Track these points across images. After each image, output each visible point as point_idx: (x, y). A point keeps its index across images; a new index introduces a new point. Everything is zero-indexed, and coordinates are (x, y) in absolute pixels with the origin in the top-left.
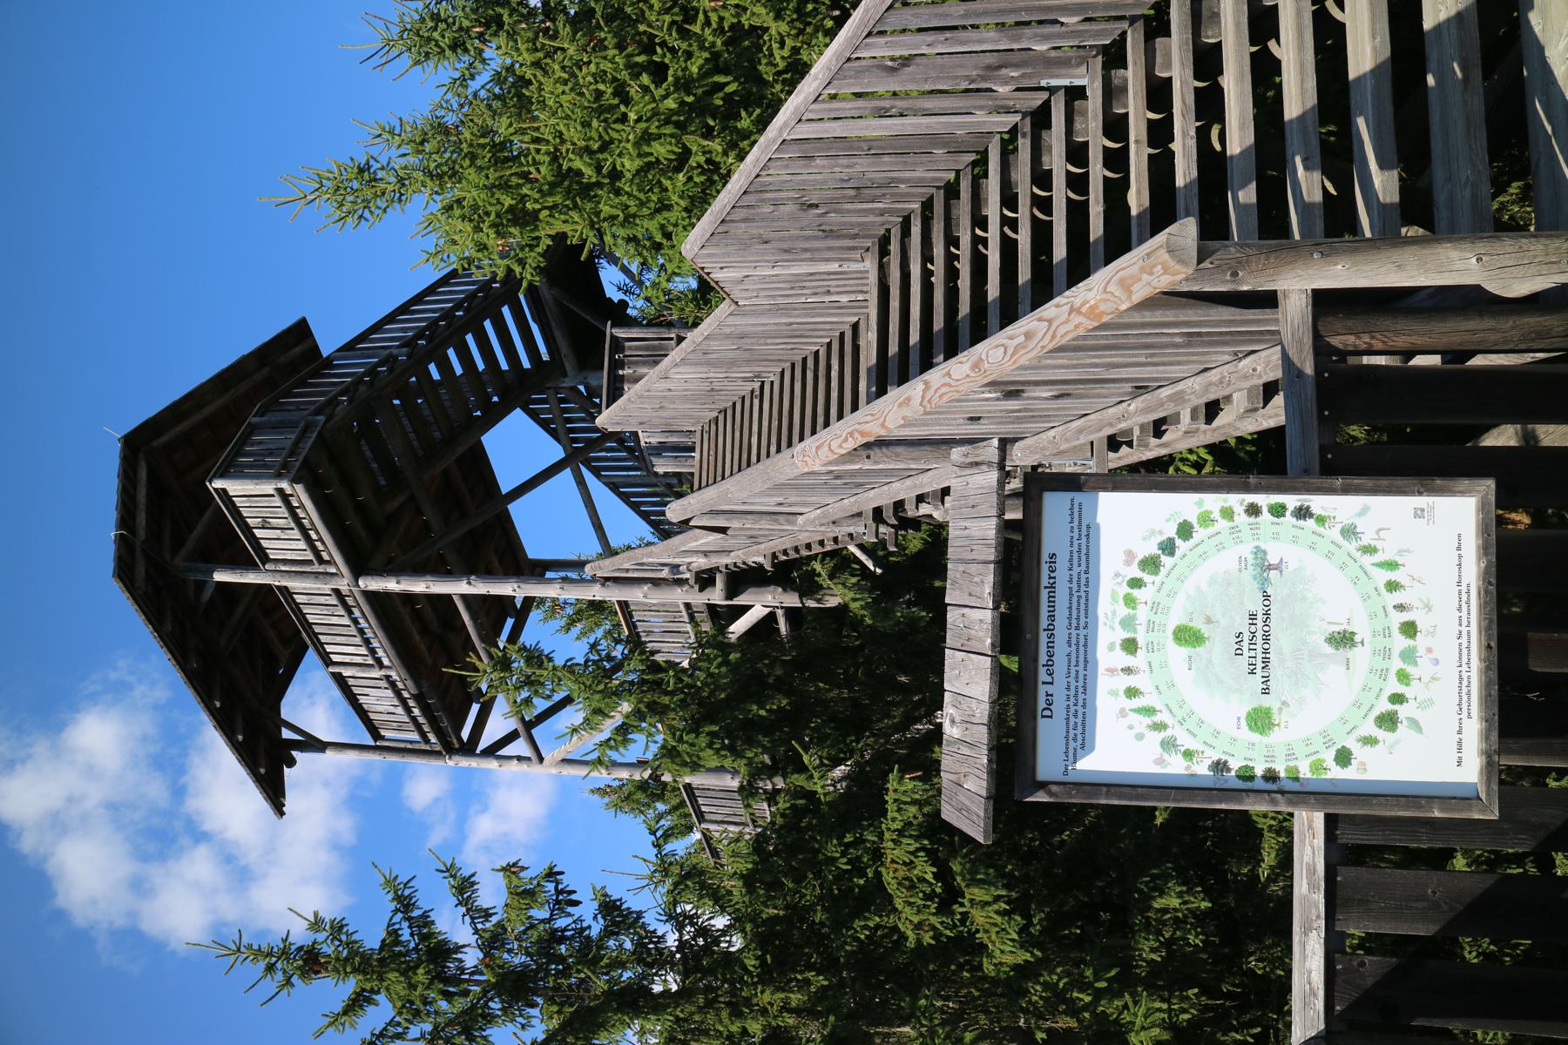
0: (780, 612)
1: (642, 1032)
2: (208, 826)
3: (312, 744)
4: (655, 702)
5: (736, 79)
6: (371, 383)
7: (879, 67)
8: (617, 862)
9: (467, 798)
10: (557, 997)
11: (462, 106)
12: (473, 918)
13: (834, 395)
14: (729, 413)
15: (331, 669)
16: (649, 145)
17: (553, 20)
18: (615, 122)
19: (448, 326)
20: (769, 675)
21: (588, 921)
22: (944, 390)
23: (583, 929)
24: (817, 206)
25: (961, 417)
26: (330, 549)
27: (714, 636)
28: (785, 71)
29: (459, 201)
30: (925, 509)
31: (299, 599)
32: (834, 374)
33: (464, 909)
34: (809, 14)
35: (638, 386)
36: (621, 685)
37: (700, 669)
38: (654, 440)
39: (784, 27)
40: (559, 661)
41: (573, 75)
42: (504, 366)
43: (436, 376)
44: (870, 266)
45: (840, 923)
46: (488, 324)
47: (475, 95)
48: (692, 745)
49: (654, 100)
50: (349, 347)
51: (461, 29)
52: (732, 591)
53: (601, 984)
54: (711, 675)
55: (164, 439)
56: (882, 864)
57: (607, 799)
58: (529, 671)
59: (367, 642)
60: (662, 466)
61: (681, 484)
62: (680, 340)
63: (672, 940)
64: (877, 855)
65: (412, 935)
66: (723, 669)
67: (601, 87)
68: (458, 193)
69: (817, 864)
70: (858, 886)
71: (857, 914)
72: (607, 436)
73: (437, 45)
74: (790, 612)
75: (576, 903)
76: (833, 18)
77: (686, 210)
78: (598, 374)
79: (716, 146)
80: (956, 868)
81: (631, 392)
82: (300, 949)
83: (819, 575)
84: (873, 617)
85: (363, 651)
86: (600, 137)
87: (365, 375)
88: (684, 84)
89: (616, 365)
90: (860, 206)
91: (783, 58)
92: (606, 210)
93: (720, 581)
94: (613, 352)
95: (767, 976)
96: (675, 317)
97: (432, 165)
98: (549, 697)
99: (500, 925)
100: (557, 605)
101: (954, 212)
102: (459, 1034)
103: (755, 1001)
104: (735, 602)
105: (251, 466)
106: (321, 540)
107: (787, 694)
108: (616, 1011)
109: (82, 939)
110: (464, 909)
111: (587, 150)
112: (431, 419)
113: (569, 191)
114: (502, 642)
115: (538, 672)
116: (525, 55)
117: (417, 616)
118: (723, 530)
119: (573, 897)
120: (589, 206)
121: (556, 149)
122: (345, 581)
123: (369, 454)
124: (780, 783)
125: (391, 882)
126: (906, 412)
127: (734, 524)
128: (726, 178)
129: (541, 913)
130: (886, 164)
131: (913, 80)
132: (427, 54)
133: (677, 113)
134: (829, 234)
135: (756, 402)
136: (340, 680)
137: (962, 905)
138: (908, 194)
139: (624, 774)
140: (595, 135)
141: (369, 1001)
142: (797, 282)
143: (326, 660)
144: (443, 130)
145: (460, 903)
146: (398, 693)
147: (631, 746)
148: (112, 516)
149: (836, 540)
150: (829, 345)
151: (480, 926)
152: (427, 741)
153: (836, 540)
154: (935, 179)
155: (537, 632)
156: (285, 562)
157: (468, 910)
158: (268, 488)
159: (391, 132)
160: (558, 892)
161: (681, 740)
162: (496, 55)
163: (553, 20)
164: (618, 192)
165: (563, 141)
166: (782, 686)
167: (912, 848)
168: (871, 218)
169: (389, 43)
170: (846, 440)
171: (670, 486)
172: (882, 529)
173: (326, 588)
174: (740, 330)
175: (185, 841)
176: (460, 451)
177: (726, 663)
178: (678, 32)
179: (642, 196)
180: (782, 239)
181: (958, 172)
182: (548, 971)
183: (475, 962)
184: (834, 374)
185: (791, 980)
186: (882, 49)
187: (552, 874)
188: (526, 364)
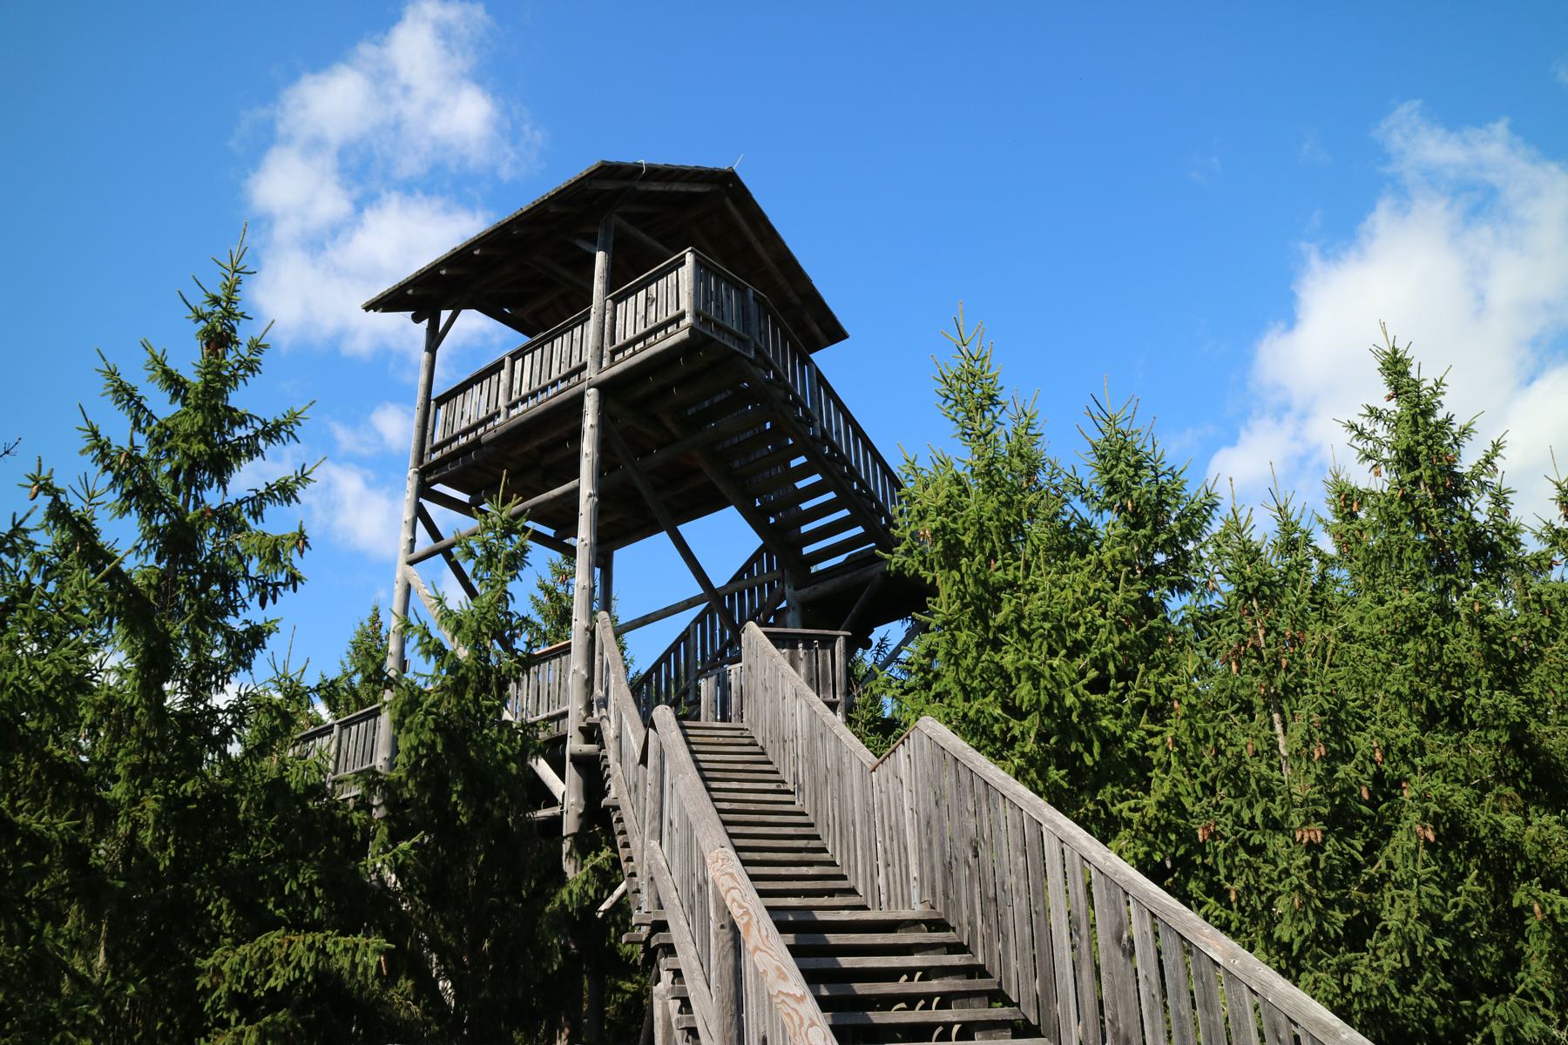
0: (557, 810)
1: (122, 671)
2: (369, 216)
3: (434, 339)
4: (467, 684)
5: (1096, 763)
6: (786, 402)
7: (1121, 924)
8: (305, 641)
9: (377, 468)
10: (167, 581)
11: (1056, 488)
12: (253, 499)
13: (783, 871)
14: (761, 758)
15: (507, 360)
16: (1028, 679)
17: (1143, 578)
18: (1050, 646)
19: (843, 476)
20: (494, 804)
21: (244, 615)
22: (796, 1018)
23: (235, 610)
24: (976, 856)
25: (766, 1028)
26: (625, 362)
27: (534, 746)
28: (1107, 813)
29: (965, 491)
30: (667, 977)
31: (578, 331)
32: (804, 870)
33: (262, 490)
34: (1165, 836)
35: (787, 666)
36: (486, 649)
37: (500, 731)
38: (732, 678)
39: (1151, 812)
40: (511, 587)
41: (1091, 601)
42: (805, 529)
43: (794, 463)
44: (917, 910)
45: (227, 882)
46: (845, 513)
47: (1066, 501)
48: (422, 725)
49: (1073, 682)
50: (821, 380)
51: (1129, 489)
52: (580, 761)
53: (178, 628)
54: (494, 743)
55: (732, 208)
56: (288, 930)
57: (367, 624)
58: (502, 556)
59: (534, 395)
60: (707, 687)
61: (689, 704)
62: (832, 706)
63: (219, 700)
64: (298, 924)
65: (240, 438)
66: (500, 757)
67: (1082, 629)
68: (973, 490)
69: (292, 857)
70: (266, 903)
71: (236, 903)
72: (737, 631)
73: (1113, 467)
74: (557, 821)
75: (263, 604)
76: (1163, 861)
77: (965, 715)
78: (798, 622)
79: (1030, 746)
80: (281, 1016)
81: (780, 657)
82: (233, 329)
83: (597, 855)
84: (553, 913)
85: (525, 391)
86: (1034, 631)
87: (795, 395)
88: (1088, 711)
89: (808, 641)
90: (977, 901)
91: (1121, 811)
92: (963, 636)
93: (591, 748)
94: (821, 638)
95: (174, 806)
96: (857, 700)
97: (999, 466)
98: (475, 576)
99: (245, 527)
100: (566, 576)
101: (975, 1002)
102: (134, 484)
103: (148, 792)
104: (568, 764)
105: (706, 289)
106: (635, 353)
107: (473, 822)
108: (146, 645)
109: (270, 93)
110: (262, 490)
111: (1020, 617)
112: (752, 458)
113: (980, 598)
114: (531, 524)
115: (501, 566)
116: (1109, 554)
117: (559, 443)
118: (644, 760)
119: (269, 601)
120: (966, 618)
121: (1020, 587)
122: (593, 376)
123: (717, 399)
124: (378, 814)
125: (294, 418)
126: (771, 976)
127: (651, 773)
128: (997, 756)
129: (254, 568)
130: (1022, 930)
131: (1109, 958)
132: (1104, 457)
133: (1061, 706)
134: (948, 869)
135: (773, 786)
136: (497, 367)
137: (238, 1021)
138: (991, 952)
139: (393, 647)
140: (1036, 624)
141: (175, 395)
142: (897, 832)
143: (517, 355)
144: (1030, 474)
145: (269, 487)
146: (483, 423)
147: (422, 659)
148: (660, 160)
149: (633, 875)
150: (833, 864)
151: (244, 506)
152: (434, 450)
153: (633, 875)
154: (1008, 981)
155: (541, 559)
156: (614, 318)
157: (262, 495)
158: (686, 304)
159: (1029, 426)
160: (275, 586)
161: (428, 713)
162: (1107, 524)
163: (1143, 578)
164: (980, 646)
165: (1027, 592)
166: (480, 816)
167: (304, 963)
168: (965, 913)
169: (1111, 421)
170: (741, 907)
171: (686, 693)
172: (645, 930)
173: (587, 357)
174: (847, 772)
175: (357, 192)
176: (721, 486)
177: (507, 759)
178: (1139, 703)
179: (977, 671)
180: (940, 820)
181: (1018, 1005)
182: (193, 573)
183: (208, 502)
184: (804, 870)
185: (167, 830)
186: (1138, 928)
187: (294, 579)
188: (807, 550)
